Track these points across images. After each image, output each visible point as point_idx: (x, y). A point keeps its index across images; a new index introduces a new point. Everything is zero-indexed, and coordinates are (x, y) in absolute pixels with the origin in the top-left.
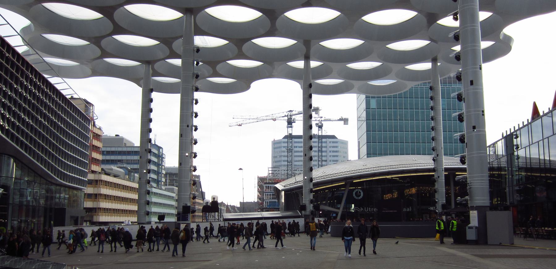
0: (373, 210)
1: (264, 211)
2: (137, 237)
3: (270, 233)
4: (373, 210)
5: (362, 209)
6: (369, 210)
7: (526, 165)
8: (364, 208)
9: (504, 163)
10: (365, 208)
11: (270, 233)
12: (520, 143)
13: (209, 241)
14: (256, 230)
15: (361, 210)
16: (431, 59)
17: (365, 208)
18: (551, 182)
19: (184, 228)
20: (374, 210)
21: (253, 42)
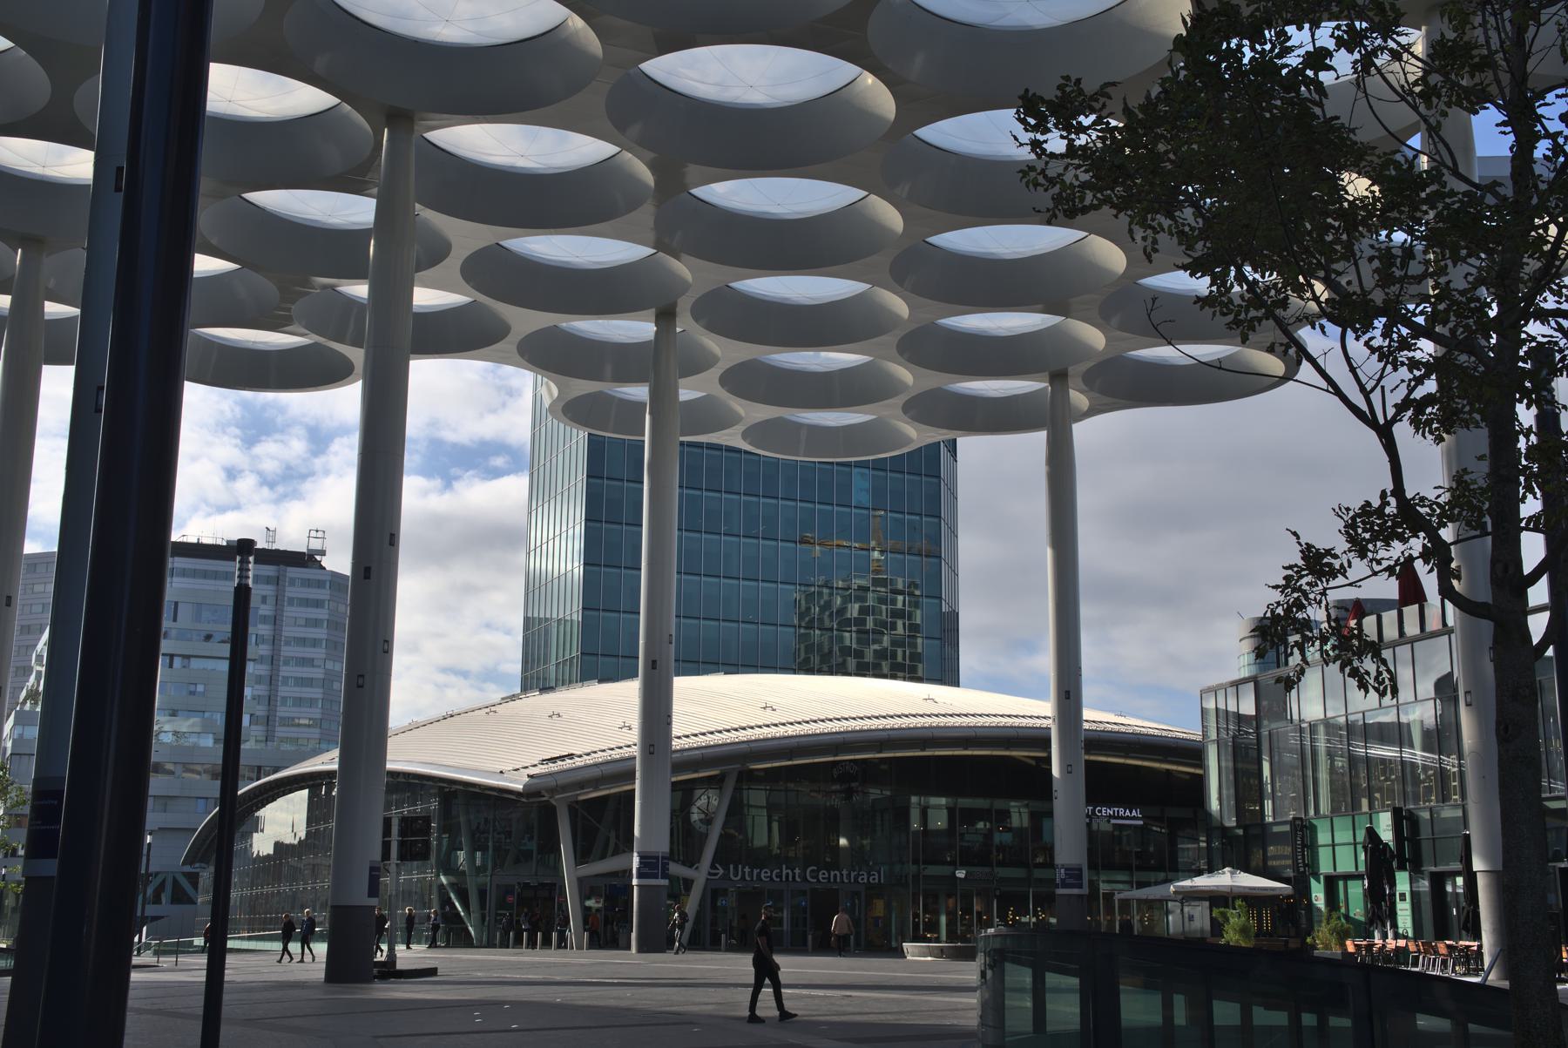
0: (759, 875)
1: (886, 670)
2: (1051, 152)
3: (1340, 329)
4: (759, 875)
5: (721, 871)
6: (744, 873)
7: (1401, 751)
8: (727, 869)
9: (308, 652)
10: (731, 866)
11: (1340, 329)
12: (1335, 834)
13: (1119, 216)
14: (1400, 402)
15: (716, 874)
16: (652, 311)
17: (731, 866)
18: (1030, 765)
19: (677, 319)
20: (763, 875)
21: (695, 197)
